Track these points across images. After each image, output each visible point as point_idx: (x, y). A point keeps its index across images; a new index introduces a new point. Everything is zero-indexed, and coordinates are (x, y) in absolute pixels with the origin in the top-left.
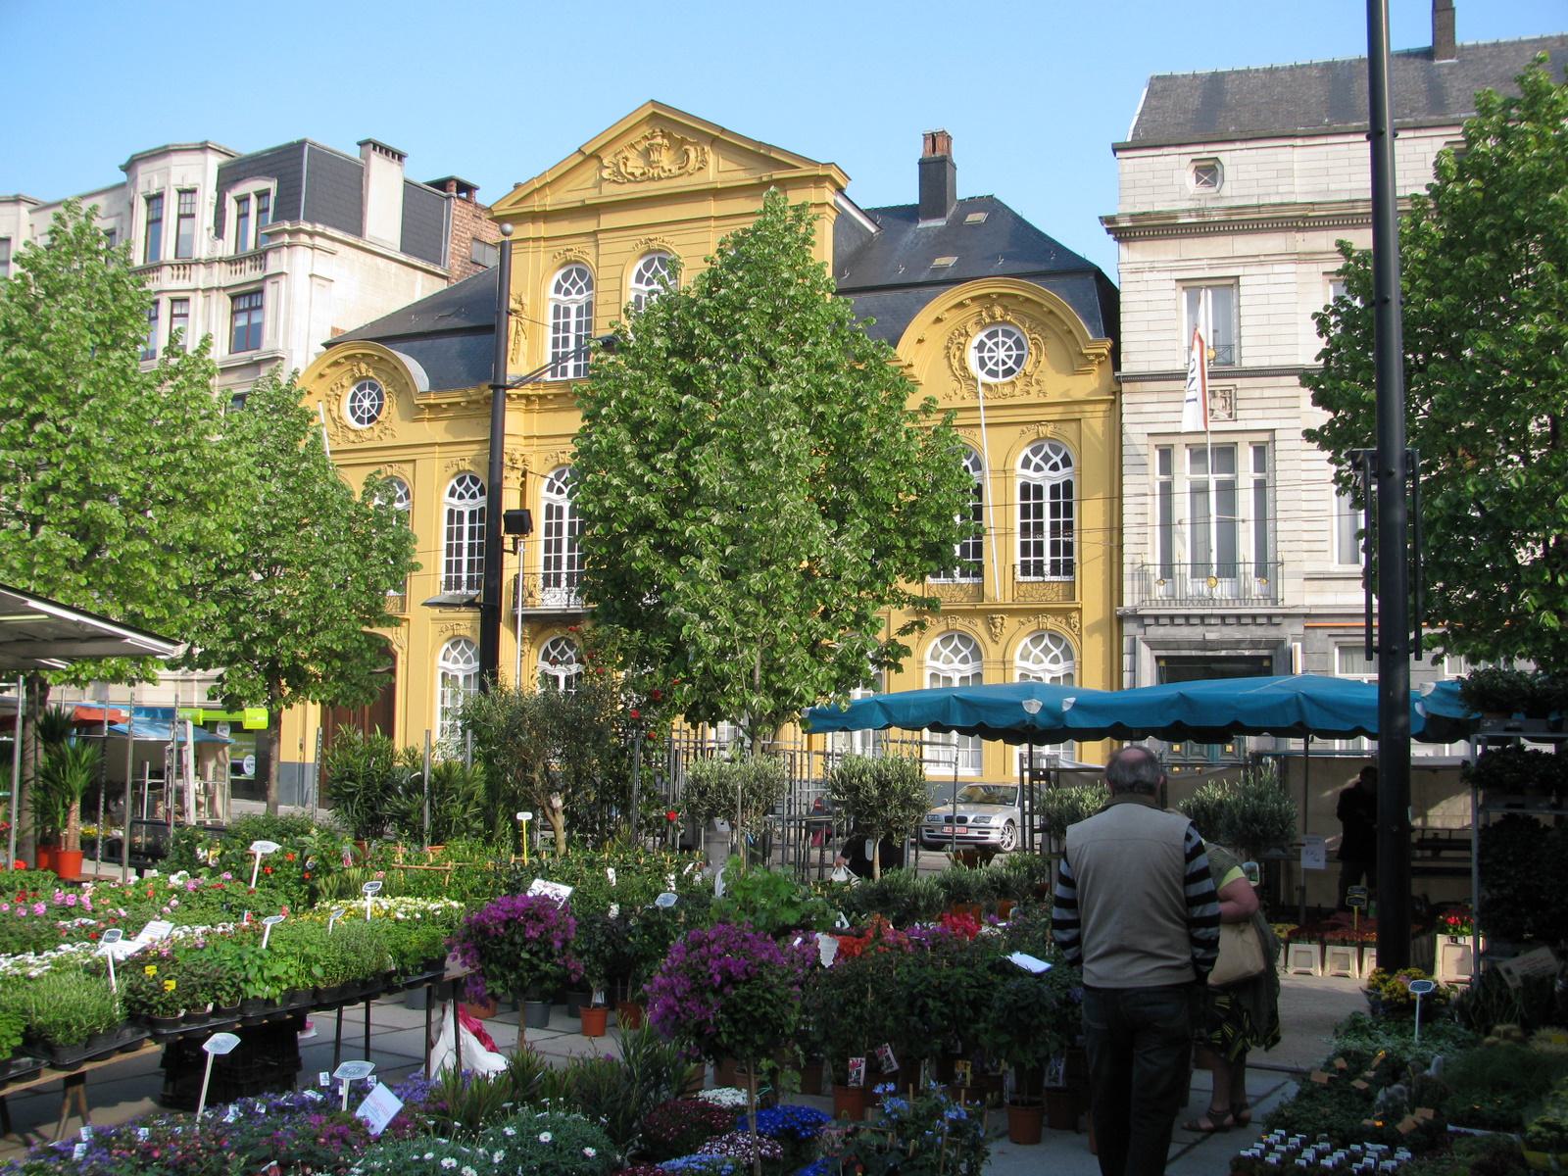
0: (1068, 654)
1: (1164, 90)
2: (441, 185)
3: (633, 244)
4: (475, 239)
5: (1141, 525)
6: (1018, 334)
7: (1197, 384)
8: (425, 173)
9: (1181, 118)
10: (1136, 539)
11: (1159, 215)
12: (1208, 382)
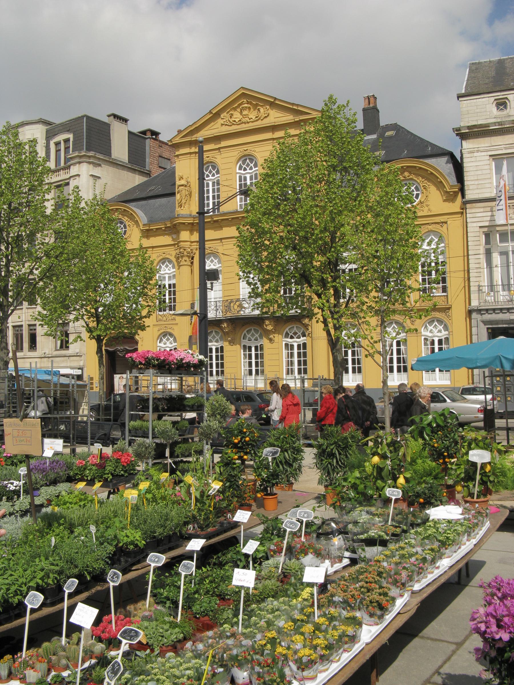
0: (446, 328)
1: (477, 69)
2: (144, 133)
3: (237, 152)
4: (160, 156)
5: (477, 268)
6: (416, 184)
7: (503, 202)
8: (137, 128)
9: (487, 81)
10: (476, 275)
11: (481, 126)
12: (508, 202)
